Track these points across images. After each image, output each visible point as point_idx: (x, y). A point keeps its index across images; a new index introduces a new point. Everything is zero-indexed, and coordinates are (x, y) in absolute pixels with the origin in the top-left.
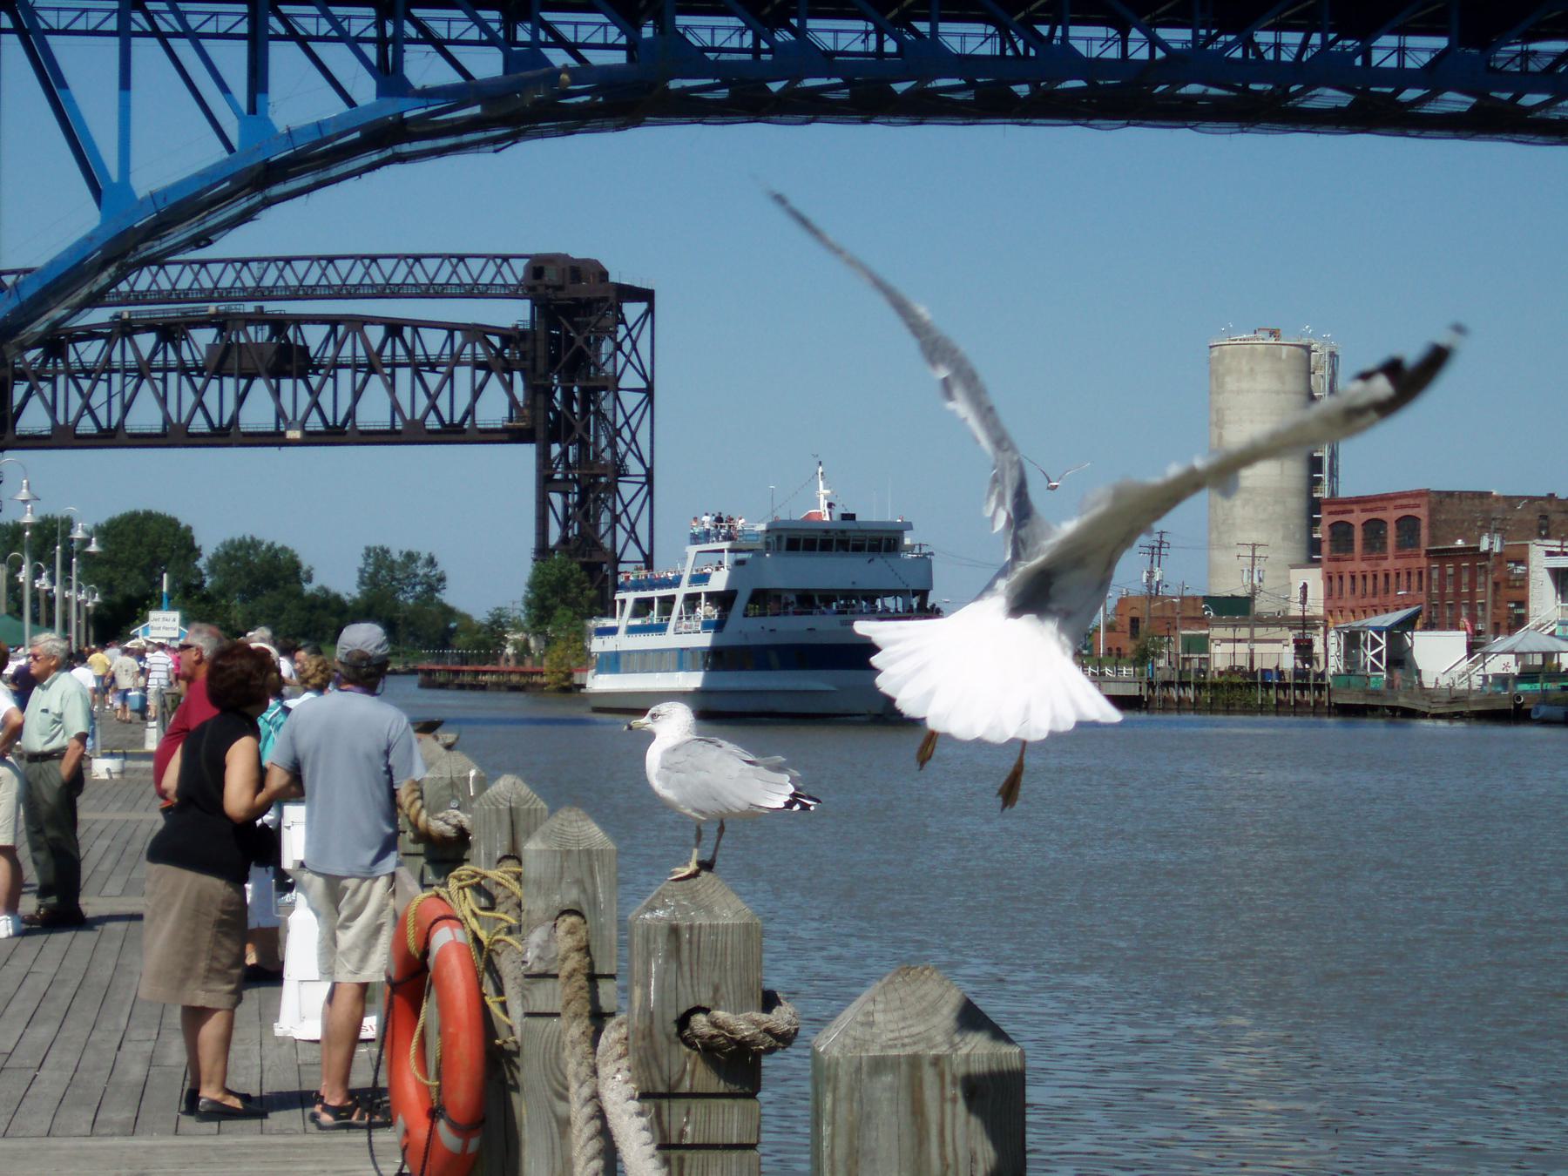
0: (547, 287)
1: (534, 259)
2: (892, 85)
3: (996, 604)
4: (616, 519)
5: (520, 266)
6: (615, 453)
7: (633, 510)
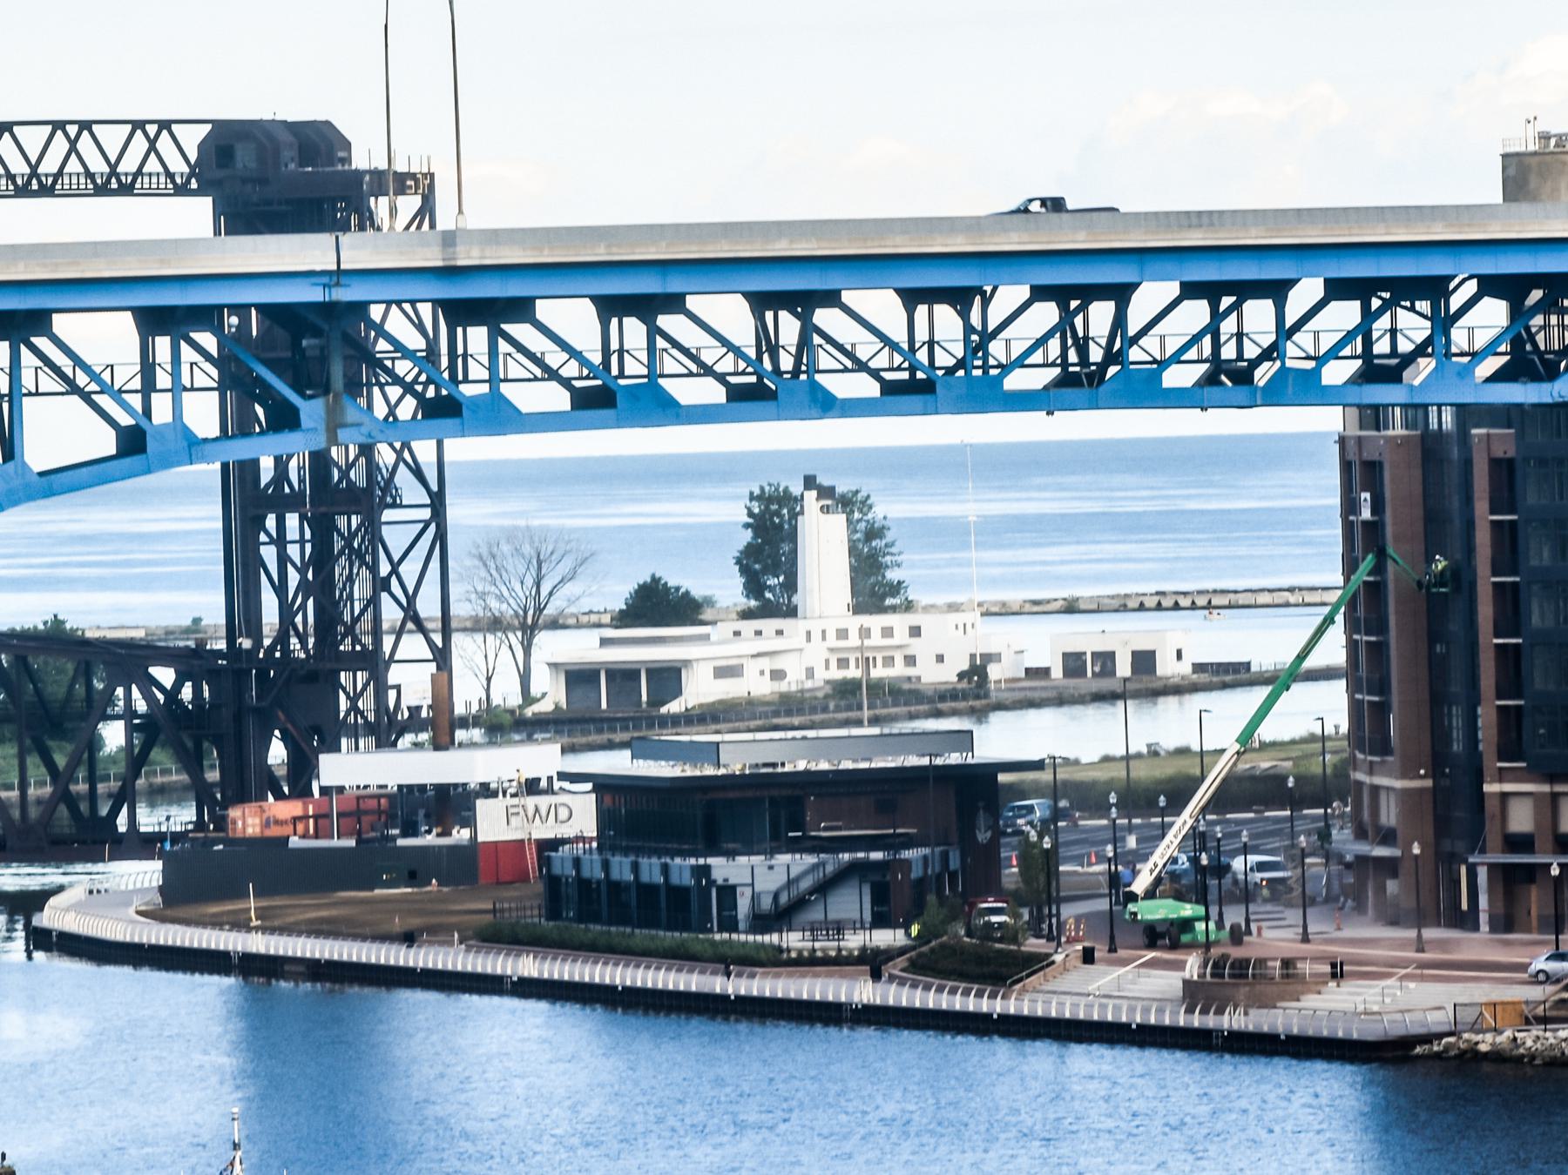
0: (244, 181)
1: (217, 125)
2: (1234, 298)
3: (718, 605)
4: (382, 585)
5: (192, 138)
6: (372, 467)
7: (409, 571)
